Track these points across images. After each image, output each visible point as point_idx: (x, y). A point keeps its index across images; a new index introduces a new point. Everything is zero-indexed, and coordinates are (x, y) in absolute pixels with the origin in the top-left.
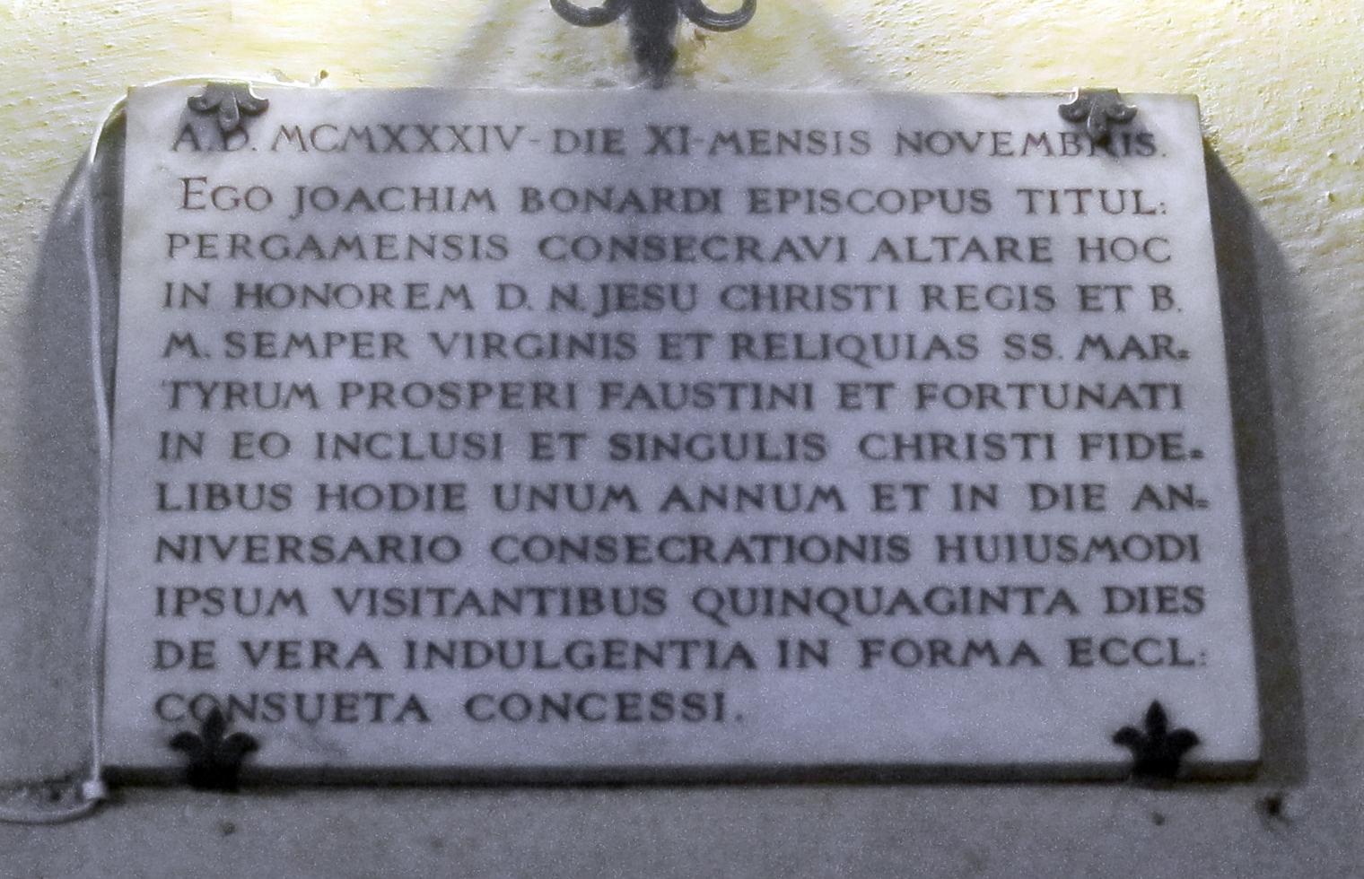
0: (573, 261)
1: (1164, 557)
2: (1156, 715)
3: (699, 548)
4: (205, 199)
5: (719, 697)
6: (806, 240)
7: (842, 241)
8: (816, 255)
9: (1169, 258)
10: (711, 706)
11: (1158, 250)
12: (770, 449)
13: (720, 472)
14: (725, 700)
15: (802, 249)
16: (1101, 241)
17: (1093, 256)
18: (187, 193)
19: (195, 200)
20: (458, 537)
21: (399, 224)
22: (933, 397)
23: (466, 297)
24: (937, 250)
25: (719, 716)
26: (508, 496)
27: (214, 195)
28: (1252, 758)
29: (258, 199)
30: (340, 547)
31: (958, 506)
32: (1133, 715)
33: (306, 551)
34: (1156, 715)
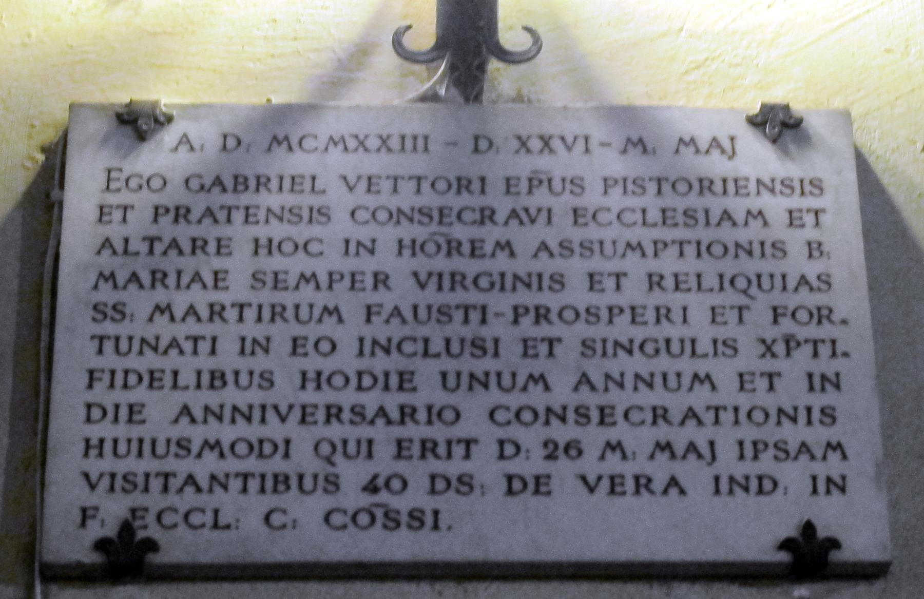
0: (372, 224)
1: (261, 455)
2: (809, 528)
3: (605, 416)
4: (120, 184)
5: (436, 513)
6: (526, 210)
7: (549, 211)
8: (533, 221)
9: (321, 253)
10: (429, 520)
11: (314, 248)
12: (700, 350)
13: (637, 364)
14: (440, 516)
15: (523, 215)
16: (270, 241)
17: (263, 251)
18: (109, 180)
19: (113, 186)
20: (460, 408)
21: (271, 199)
22: (784, 315)
23: (763, 218)
24: (144, 248)
25: (436, 527)
26: (452, 381)
27: (127, 181)
28: (829, 556)
29: (156, 183)
30: (370, 413)
31: (811, 388)
32: (789, 529)
33: (346, 415)
34: (809, 528)
